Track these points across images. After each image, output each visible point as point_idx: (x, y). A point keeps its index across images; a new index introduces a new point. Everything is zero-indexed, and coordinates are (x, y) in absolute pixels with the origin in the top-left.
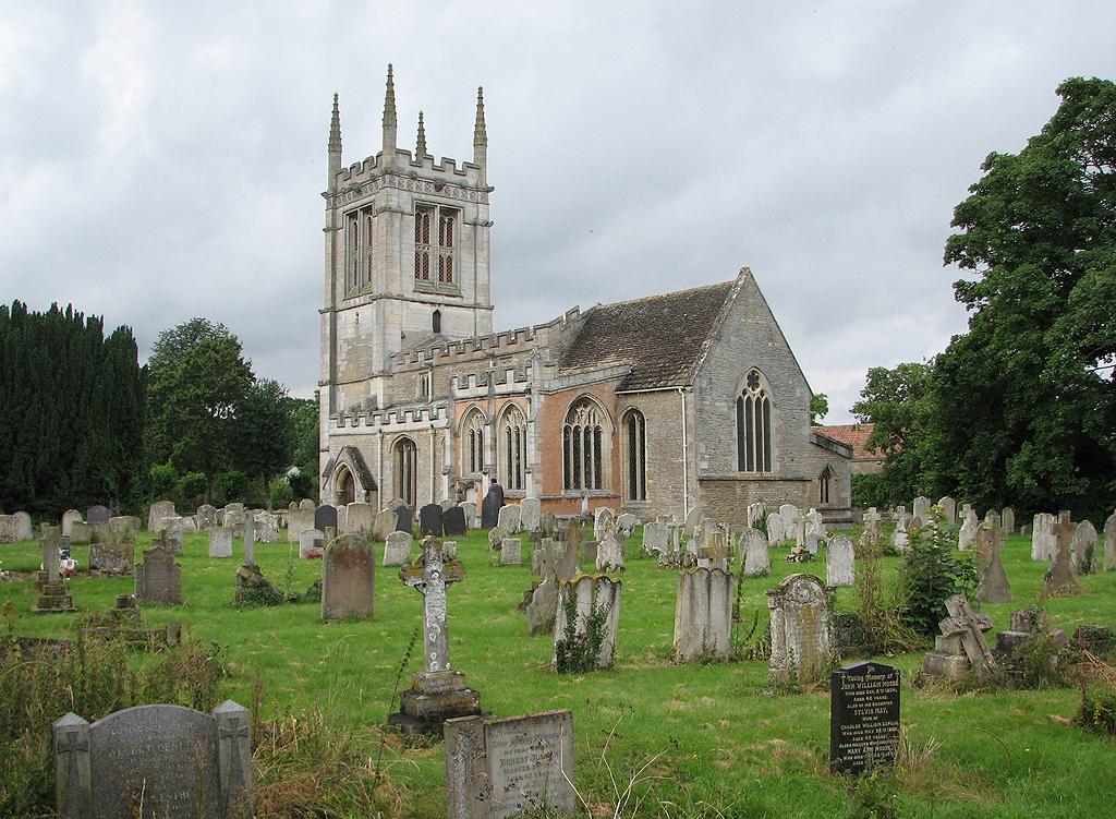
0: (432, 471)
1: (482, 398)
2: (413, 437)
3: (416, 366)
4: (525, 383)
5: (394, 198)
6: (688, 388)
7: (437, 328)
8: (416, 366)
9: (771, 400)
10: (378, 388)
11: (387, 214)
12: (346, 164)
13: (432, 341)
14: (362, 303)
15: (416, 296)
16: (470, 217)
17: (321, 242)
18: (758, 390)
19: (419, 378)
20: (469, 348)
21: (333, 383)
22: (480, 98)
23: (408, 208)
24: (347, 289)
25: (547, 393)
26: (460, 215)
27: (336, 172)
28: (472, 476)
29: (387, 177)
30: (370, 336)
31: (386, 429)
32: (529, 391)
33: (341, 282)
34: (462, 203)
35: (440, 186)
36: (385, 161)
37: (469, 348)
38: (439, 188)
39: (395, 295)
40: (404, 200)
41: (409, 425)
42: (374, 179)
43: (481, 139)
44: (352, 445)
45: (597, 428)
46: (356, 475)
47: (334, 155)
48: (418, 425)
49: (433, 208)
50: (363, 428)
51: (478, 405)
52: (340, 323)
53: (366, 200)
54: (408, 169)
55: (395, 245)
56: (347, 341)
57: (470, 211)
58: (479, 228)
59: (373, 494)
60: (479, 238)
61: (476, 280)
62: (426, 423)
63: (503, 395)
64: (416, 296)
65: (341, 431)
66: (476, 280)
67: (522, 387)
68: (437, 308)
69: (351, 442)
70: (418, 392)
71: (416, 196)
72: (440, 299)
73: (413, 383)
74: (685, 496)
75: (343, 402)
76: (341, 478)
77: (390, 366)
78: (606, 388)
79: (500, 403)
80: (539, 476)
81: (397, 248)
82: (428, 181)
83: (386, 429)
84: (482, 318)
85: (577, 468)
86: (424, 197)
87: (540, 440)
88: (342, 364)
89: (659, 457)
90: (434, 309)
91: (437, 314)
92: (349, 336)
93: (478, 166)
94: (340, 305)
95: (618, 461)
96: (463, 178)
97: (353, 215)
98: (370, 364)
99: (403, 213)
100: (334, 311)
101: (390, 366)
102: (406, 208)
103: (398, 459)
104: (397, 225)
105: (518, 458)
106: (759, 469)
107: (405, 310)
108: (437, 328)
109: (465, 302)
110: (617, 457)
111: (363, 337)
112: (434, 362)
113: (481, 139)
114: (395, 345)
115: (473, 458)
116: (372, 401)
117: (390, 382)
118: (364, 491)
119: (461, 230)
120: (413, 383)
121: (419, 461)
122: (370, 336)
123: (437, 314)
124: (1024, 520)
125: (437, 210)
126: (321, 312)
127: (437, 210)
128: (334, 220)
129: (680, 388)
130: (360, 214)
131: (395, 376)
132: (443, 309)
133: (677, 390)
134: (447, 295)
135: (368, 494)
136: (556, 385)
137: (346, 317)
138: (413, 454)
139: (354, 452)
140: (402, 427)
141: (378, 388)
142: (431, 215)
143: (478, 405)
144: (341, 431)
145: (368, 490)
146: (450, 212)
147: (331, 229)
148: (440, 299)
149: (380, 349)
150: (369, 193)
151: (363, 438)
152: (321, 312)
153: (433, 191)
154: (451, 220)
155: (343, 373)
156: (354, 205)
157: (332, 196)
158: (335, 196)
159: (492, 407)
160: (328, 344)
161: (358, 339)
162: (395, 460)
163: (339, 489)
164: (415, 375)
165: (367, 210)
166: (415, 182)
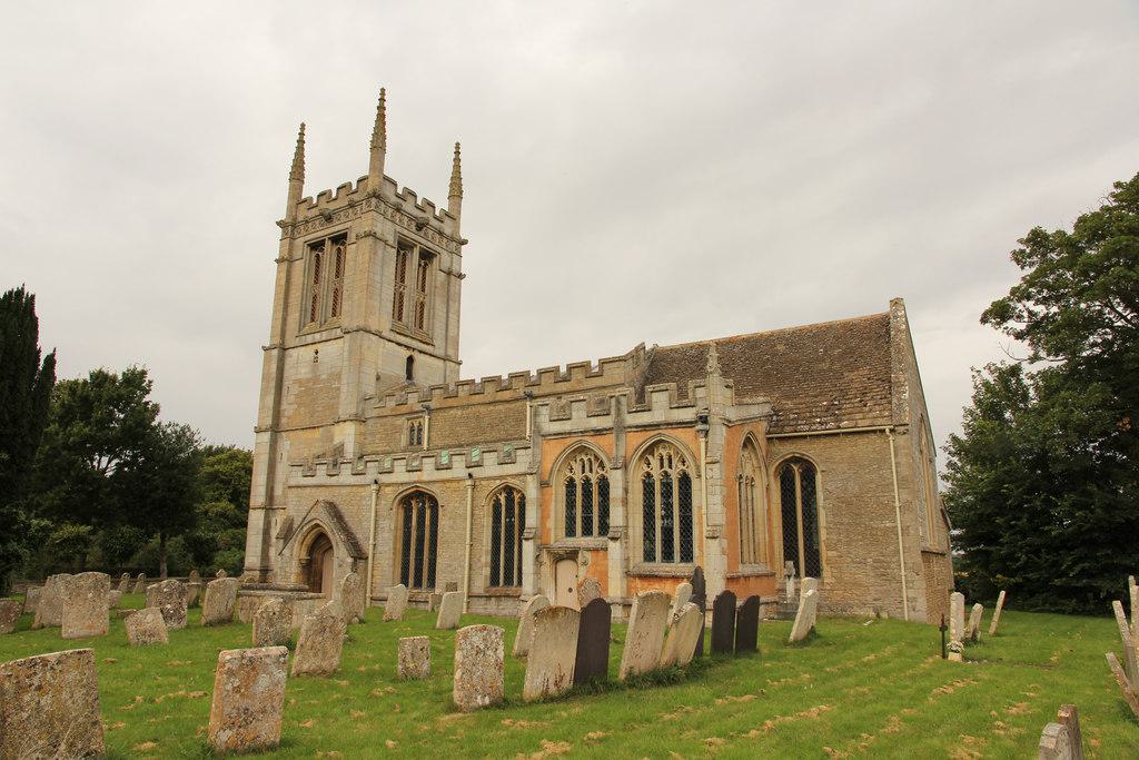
0: (468, 536)
1: (598, 432)
2: (435, 490)
3: (404, 409)
4: (693, 410)
5: (379, 225)
7: (409, 375)
8: (404, 409)
10: (347, 435)
11: (370, 240)
12: (310, 190)
13: (405, 387)
14: (324, 339)
15: (392, 336)
16: (445, 266)
17: (269, 275)
19: (407, 425)
20: (490, 388)
21: (275, 429)
22: (457, 153)
23: (391, 239)
24: (301, 325)
25: (728, 423)
26: (435, 261)
27: (297, 200)
28: (571, 542)
29: (374, 201)
31: (385, 479)
33: (294, 317)
34: (439, 249)
35: (421, 226)
36: (371, 186)
37: (490, 388)
38: (420, 227)
39: (373, 329)
40: (388, 230)
41: (428, 473)
42: (352, 205)
43: (456, 191)
44: (329, 499)
46: (337, 538)
49: (412, 248)
51: (590, 441)
52: (289, 362)
54: (394, 199)
55: (369, 274)
56: (299, 382)
57: (444, 259)
58: (453, 277)
59: (361, 564)
60: (452, 289)
61: (447, 331)
62: (459, 469)
64: (392, 336)
66: (447, 331)
67: (688, 415)
69: (323, 495)
70: (404, 440)
71: (398, 229)
72: (415, 344)
73: (398, 429)
76: (309, 540)
77: (363, 410)
79: (636, 440)
81: (378, 278)
82: (412, 218)
83: (385, 479)
84: (451, 371)
85: (420, 551)
86: (405, 232)
88: (288, 408)
90: (409, 353)
91: (410, 360)
93: (452, 216)
94: (290, 342)
96: (400, 201)
97: (316, 246)
99: (385, 242)
100: (283, 349)
101: (363, 410)
102: (367, 247)
104: (380, 252)
105: (668, 515)
106: (668, 556)
107: (381, 349)
108: (409, 375)
109: (437, 352)
112: (433, 405)
113: (456, 191)
114: (370, 388)
117: (362, 428)
118: (350, 560)
119: (436, 276)
120: (398, 429)
123: (410, 360)
124: (693, 601)
125: (416, 251)
126: (265, 349)
127: (416, 251)
128: (290, 251)
131: (370, 422)
132: (417, 356)
134: (421, 341)
137: (300, 360)
138: (428, 512)
139: (334, 511)
141: (347, 435)
143: (590, 441)
145: (355, 559)
146: (427, 256)
147: (286, 261)
148: (415, 344)
150: (343, 219)
151: (344, 491)
152: (265, 349)
153: (414, 229)
154: (426, 264)
155: (289, 418)
156: (320, 234)
157: (290, 227)
158: (294, 225)
159: (622, 444)
160: (273, 384)
161: (316, 379)
162: (397, 521)
163: (304, 555)
164: (401, 421)
165: (339, 239)
166: (398, 215)
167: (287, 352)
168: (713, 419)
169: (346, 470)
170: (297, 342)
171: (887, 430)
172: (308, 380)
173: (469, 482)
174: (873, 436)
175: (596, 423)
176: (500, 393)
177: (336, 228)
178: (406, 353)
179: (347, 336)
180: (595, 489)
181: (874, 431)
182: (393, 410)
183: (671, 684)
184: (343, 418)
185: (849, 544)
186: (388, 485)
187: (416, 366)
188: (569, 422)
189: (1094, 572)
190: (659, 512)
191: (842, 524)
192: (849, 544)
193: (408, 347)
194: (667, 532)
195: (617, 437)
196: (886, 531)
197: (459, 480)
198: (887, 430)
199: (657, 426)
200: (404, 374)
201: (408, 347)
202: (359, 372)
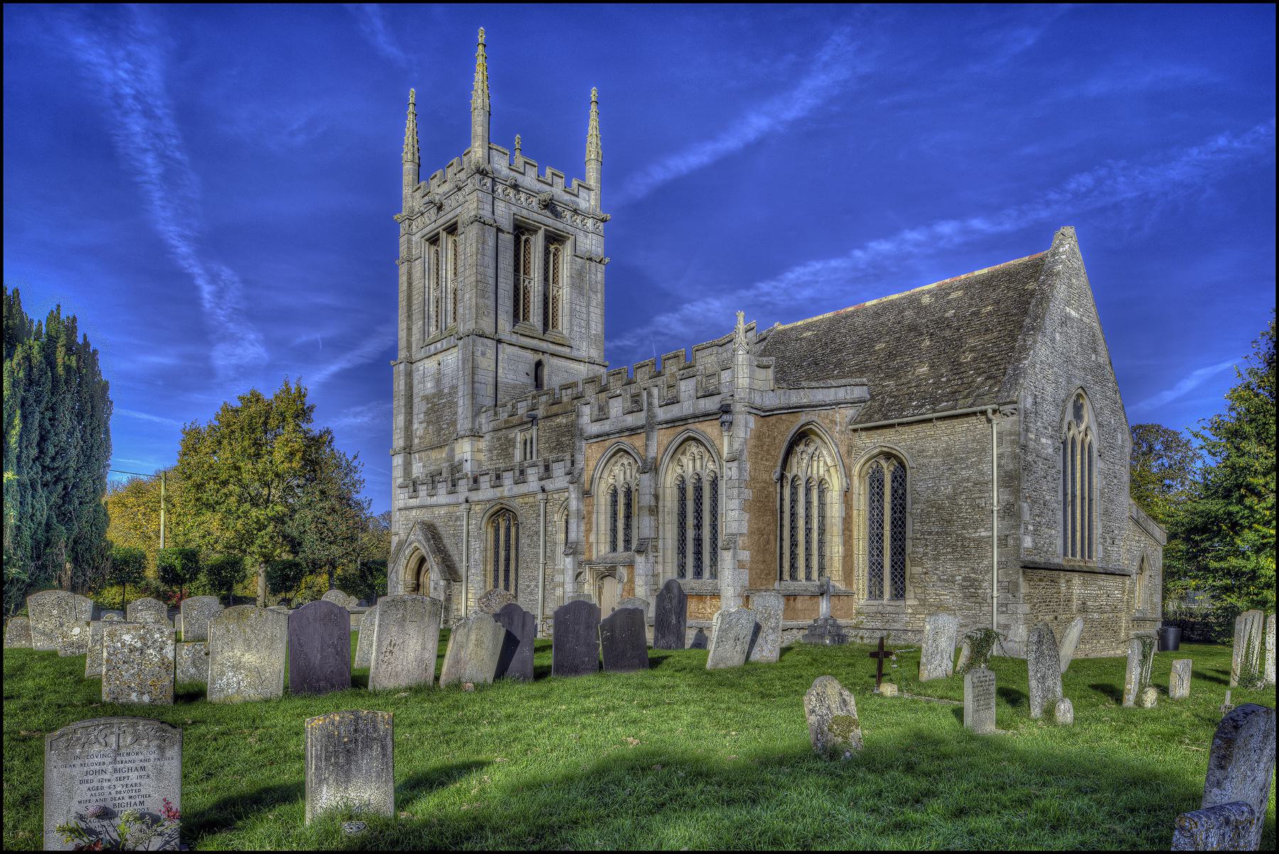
3: (515, 420)
6: (1008, 409)
9: (1095, 446)
15: (514, 338)
18: (1083, 427)
30: (454, 388)
32: (726, 409)
45: (821, 482)
47: (455, 773)
48: (522, 489)
50: (442, 497)
52: (417, 378)
53: (450, 216)
56: (426, 398)
59: (455, 586)
62: (533, 483)
63: (672, 423)
64: (514, 338)
65: (413, 502)
67: (711, 404)
68: (540, 356)
72: (544, 346)
74: (995, 594)
75: (418, 470)
78: (838, 418)
80: (745, 555)
83: (474, 496)
86: (525, 212)
87: (748, 494)
89: (935, 529)
91: (539, 364)
92: (427, 392)
95: (851, 537)
96: (573, 198)
98: (453, 423)
103: (491, 537)
105: (698, 526)
110: (851, 531)
111: (446, 391)
115: (614, 530)
116: (455, 468)
118: (442, 583)
121: (524, 541)
122: (454, 388)
123: (539, 364)
125: (541, 233)
127: (541, 233)
129: (989, 408)
130: (443, 235)
132: (545, 358)
133: (984, 413)
135: (448, 586)
136: (771, 401)
138: (513, 530)
139: (431, 532)
140: (498, 492)
142: (532, 238)
143: (626, 442)
144: (413, 502)
148: (544, 346)
149: (468, 402)
161: (439, 394)
167: (414, 366)
168: (738, 407)
169: (423, 490)
170: (422, 354)
171: (990, 411)
172: (434, 396)
173: (540, 496)
174: (973, 420)
175: (630, 420)
176: (702, 401)
177: (446, 218)
178: (532, 357)
179: (460, 343)
180: (621, 500)
181: (974, 414)
182: (506, 422)
183: (40, 806)
184: (462, 433)
185: (936, 559)
186: (478, 502)
187: (546, 371)
188: (607, 422)
189: (322, 684)
190: (690, 521)
191: (930, 533)
192: (936, 559)
193: (535, 350)
194: (698, 541)
195: (648, 439)
196: (979, 542)
197: (534, 494)
198: (990, 411)
199: (684, 420)
200: (530, 381)
201: (535, 350)
202: (473, 382)
